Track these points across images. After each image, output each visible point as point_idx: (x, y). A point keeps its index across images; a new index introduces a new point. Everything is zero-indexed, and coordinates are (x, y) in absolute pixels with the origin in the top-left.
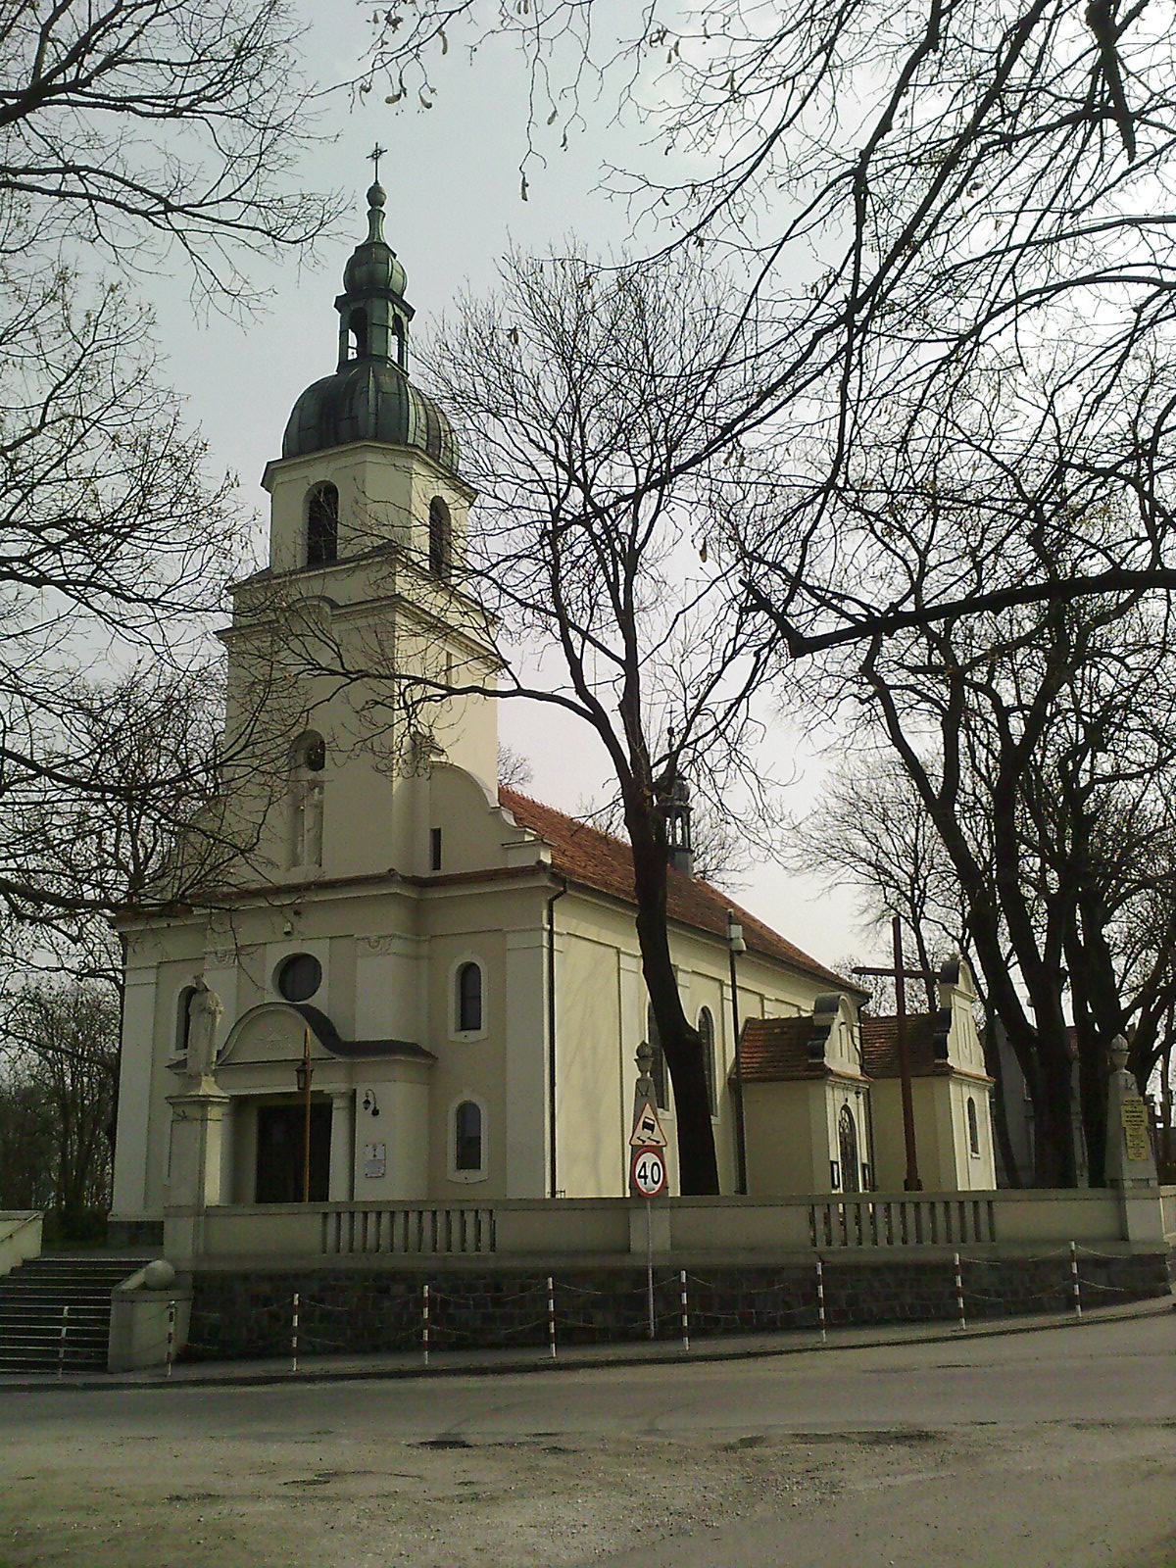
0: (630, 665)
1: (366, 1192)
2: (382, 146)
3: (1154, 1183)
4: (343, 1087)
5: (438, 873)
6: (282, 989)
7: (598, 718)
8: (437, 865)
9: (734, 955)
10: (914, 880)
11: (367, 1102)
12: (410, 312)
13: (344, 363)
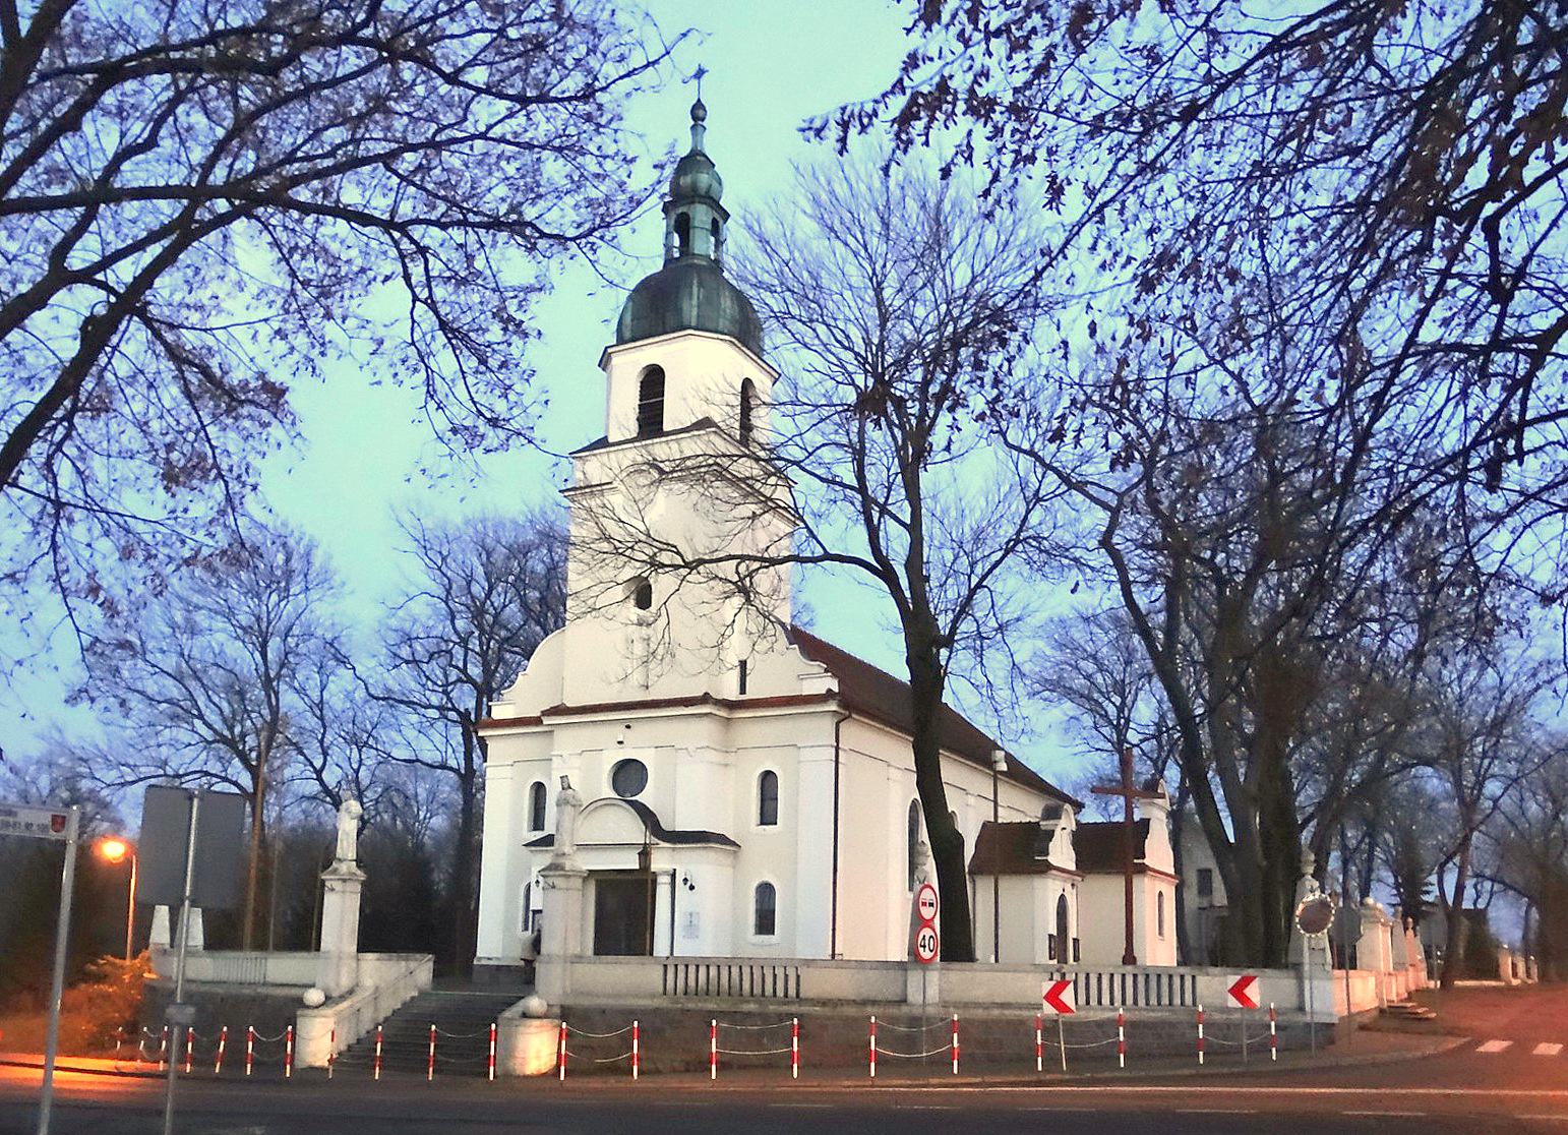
0: (914, 528)
1: (684, 949)
2: (705, 66)
3: (1329, 968)
4: (669, 867)
5: (743, 697)
6: (616, 788)
7: (886, 572)
8: (743, 691)
9: (996, 776)
10: (1120, 710)
11: (686, 880)
12: (726, 216)
13: (669, 261)
